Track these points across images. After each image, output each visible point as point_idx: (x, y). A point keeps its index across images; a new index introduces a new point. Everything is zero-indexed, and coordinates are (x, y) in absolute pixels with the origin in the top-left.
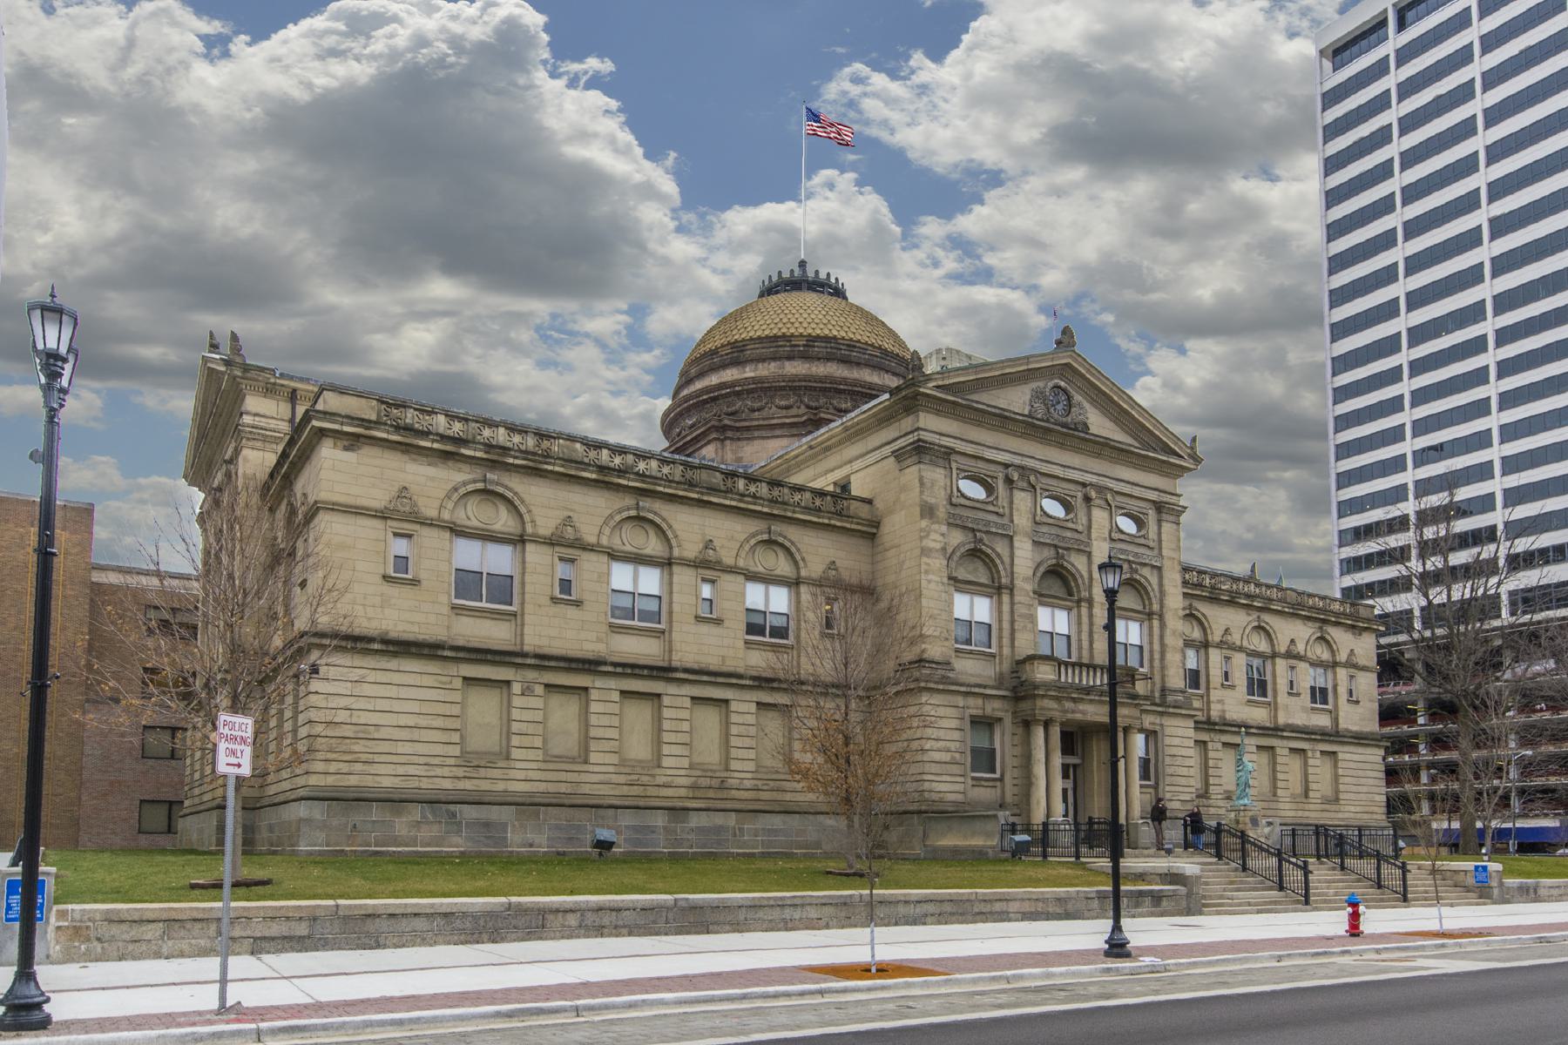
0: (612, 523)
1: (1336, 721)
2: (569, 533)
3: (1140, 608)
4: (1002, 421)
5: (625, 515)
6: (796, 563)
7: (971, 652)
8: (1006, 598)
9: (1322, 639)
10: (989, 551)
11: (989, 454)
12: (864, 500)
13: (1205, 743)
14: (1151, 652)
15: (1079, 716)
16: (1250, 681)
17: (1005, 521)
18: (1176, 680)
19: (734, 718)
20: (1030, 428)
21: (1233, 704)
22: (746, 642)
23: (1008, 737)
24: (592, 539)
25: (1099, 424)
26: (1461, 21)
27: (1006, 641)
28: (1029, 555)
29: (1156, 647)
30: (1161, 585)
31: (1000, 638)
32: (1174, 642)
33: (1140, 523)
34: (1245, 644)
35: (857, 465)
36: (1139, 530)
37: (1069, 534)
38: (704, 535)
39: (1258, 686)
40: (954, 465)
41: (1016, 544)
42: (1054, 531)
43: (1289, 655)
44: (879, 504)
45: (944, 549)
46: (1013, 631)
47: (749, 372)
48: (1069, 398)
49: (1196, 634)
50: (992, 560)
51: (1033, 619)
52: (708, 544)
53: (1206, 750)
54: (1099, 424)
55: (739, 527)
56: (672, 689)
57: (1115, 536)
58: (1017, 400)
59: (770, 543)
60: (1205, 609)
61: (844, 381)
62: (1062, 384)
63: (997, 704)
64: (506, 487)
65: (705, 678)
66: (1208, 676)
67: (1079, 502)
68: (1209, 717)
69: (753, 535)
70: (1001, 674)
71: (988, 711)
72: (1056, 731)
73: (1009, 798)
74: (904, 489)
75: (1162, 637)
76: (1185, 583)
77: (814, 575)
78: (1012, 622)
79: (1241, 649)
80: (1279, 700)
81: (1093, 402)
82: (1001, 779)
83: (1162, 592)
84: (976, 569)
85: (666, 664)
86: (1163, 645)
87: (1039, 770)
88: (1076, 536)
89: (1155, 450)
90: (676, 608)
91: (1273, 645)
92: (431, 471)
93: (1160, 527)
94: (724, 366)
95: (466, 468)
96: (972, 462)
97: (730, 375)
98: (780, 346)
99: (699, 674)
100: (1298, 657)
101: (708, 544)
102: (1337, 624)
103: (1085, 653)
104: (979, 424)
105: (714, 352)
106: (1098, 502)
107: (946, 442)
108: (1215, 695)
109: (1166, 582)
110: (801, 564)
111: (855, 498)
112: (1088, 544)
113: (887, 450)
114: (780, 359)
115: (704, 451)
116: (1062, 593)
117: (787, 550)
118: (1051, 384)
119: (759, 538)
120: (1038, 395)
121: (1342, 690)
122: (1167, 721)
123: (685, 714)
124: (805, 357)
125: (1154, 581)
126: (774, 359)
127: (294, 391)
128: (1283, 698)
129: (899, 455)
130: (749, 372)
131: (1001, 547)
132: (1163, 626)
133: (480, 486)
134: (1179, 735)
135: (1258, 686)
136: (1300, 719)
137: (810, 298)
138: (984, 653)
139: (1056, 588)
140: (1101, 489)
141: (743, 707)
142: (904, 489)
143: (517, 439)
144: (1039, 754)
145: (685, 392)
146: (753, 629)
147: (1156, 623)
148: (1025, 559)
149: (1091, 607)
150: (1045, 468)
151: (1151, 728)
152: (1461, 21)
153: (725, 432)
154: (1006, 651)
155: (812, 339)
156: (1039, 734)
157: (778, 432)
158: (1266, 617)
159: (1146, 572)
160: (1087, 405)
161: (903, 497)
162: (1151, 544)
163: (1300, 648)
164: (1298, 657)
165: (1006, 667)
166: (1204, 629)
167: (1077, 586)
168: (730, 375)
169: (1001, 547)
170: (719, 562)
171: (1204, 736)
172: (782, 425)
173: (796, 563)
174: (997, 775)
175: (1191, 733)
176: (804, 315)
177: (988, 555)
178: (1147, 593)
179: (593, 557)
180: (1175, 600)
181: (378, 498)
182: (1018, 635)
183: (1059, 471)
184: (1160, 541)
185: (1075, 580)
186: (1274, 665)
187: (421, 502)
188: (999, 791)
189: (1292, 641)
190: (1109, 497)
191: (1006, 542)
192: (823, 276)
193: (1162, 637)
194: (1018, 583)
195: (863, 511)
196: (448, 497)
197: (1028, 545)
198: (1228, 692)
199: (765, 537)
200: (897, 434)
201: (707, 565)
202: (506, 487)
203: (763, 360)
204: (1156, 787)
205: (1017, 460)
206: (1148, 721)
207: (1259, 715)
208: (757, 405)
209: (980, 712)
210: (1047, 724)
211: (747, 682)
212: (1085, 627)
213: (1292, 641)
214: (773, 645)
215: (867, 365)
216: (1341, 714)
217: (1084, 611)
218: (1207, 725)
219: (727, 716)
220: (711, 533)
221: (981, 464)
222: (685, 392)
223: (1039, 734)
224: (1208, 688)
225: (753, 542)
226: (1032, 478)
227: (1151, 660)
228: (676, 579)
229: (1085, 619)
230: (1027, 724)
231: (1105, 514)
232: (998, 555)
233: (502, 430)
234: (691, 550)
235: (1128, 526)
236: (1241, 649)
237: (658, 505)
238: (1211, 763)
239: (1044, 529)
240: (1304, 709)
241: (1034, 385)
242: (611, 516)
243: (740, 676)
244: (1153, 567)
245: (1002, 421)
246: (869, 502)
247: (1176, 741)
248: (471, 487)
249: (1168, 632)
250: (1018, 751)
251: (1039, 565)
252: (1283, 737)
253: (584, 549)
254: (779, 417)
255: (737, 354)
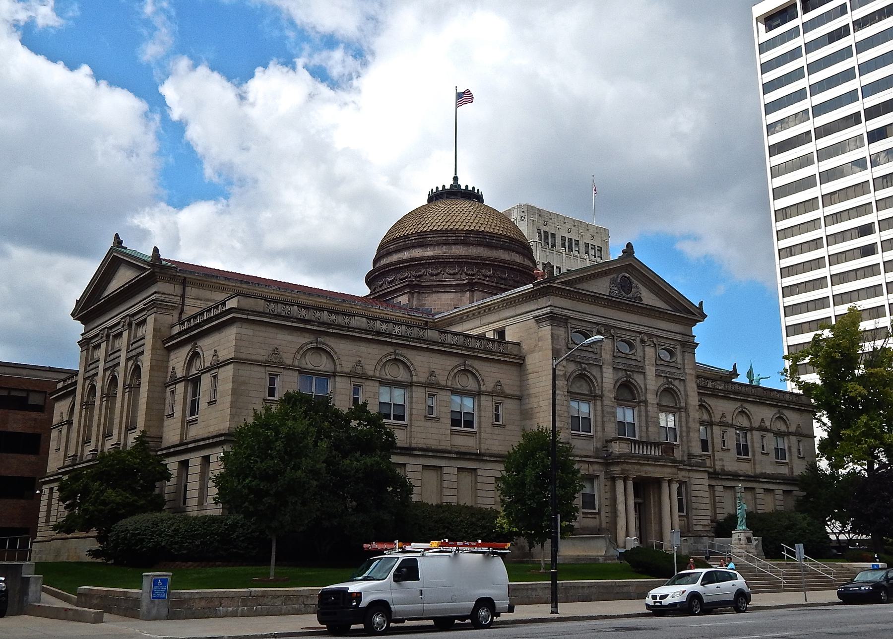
0: (381, 363)
1: (791, 469)
2: (359, 370)
3: (674, 405)
4: (595, 299)
5: (388, 358)
6: (478, 382)
7: (579, 435)
8: (599, 403)
9: (780, 418)
10: (589, 375)
11: (589, 318)
12: (514, 343)
13: (713, 486)
14: (681, 432)
15: (643, 474)
16: (738, 446)
17: (597, 357)
18: (697, 450)
19: (445, 477)
20: (609, 302)
21: (729, 462)
22: (452, 431)
23: (602, 485)
24: (371, 373)
25: (649, 298)
26: (842, 10)
27: (599, 429)
28: (611, 376)
29: (684, 429)
30: (685, 391)
31: (596, 426)
32: (694, 425)
33: (671, 353)
34: (734, 422)
35: (509, 322)
36: (671, 357)
37: (632, 362)
38: (429, 368)
39: (743, 450)
40: (569, 325)
41: (604, 370)
42: (624, 361)
43: (761, 429)
44: (524, 346)
45: (565, 374)
46: (603, 422)
47: (429, 252)
48: (631, 283)
49: (706, 417)
50: (591, 380)
51: (614, 415)
52: (432, 373)
53: (714, 491)
54: (649, 298)
55: (448, 363)
56: (412, 460)
57: (659, 362)
58: (602, 287)
59: (465, 371)
60: (711, 402)
61: (489, 259)
62: (627, 275)
63: (596, 467)
64: (327, 345)
65: (430, 454)
66: (713, 443)
67: (637, 343)
68: (715, 469)
69: (456, 367)
70: (597, 448)
71: (591, 472)
72: (630, 484)
73: (604, 525)
74: (540, 339)
75: (687, 422)
76: (699, 387)
77: (489, 390)
78: (603, 416)
79: (732, 426)
80: (756, 458)
81: (645, 285)
82: (599, 513)
83: (687, 396)
84: (581, 386)
85: (407, 446)
86: (688, 427)
87: (621, 507)
88: (637, 364)
89: (680, 312)
90: (414, 412)
91: (751, 423)
92: (289, 338)
93: (683, 356)
94: (413, 247)
95: (307, 335)
96: (579, 323)
97: (417, 253)
98: (447, 237)
99: (427, 452)
100: (766, 430)
101: (432, 373)
102: (788, 408)
103: (644, 434)
104: (583, 301)
105: (406, 237)
106: (649, 343)
107: (566, 312)
108: (718, 455)
109: (688, 388)
110: (481, 383)
111: (508, 343)
112: (643, 368)
113: (530, 316)
114: (449, 244)
115: (400, 299)
116: (629, 397)
117: (474, 374)
118: (620, 276)
119: (459, 368)
120: (613, 281)
121: (794, 450)
122: (692, 475)
123: (419, 476)
124: (465, 243)
125: (682, 389)
126: (446, 244)
127: (185, 278)
128: (759, 457)
129: (538, 320)
130: (429, 252)
131: (595, 372)
132: (688, 416)
133: (314, 345)
134: (700, 483)
135: (743, 450)
136: (770, 470)
137: (464, 205)
138: (588, 436)
139: (626, 395)
140: (650, 336)
141: (451, 471)
142: (540, 339)
143: (333, 317)
144: (620, 498)
145: (384, 262)
146: (455, 422)
147: (683, 414)
148: (608, 378)
149: (646, 406)
150: (619, 324)
151: (684, 479)
152: (842, 10)
153: (417, 288)
154: (599, 434)
155: (469, 232)
156: (620, 485)
157: (448, 289)
158: (746, 405)
159: (676, 383)
160: (640, 286)
161: (540, 344)
162: (679, 366)
163: (767, 424)
164: (766, 430)
165: (599, 445)
166: (710, 414)
167: (638, 393)
168: (417, 253)
169: (595, 372)
170: (438, 384)
171: (713, 483)
172: (451, 285)
173: (478, 382)
174: (597, 511)
175: (706, 482)
176: (461, 216)
177: (588, 377)
178: (678, 396)
179: (370, 383)
180: (694, 400)
181: (262, 354)
182: (607, 425)
183: (626, 326)
184: (684, 364)
185: (637, 390)
186: (752, 435)
187: (284, 356)
188: (598, 520)
189: (763, 419)
190: (654, 340)
191: (598, 368)
192: (470, 188)
193: (687, 422)
194: (606, 393)
195: (515, 351)
196: (298, 352)
197: (611, 370)
198: (727, 454)
199: (463, 368)
200: (536, 307)
201: (432, 386)
202: (327, 345)
203: (438, 244)
204: (687, 516)
205: (603, 321)
206: (682, 475)
207: (745, 468)
208: (434, 272)
209: (587, 473)
210: (625, 480)
211: (453, 455)
212: (644, 418)
213: (763, 419)
214: (466, 432)
215: (502, 248)
216: (795, 466)
217: (643, 408)
218: (714, 475)
219: (441, 476)
220: (433, 367)
221: (583, 324)
222: (384, 262)
223: (620, 485)
224: (713, 451)
225: (455, 371)
226: (612, 331)
227: (681, 437)
228: (414, 395)
229: (643, 414)
230: (613, 480)
231: (653, 350)
232: (594, 377)
233: (326, 313)
234: (422, 377)
235: (666, 356)
236: (732, 426)
237: (404, 352)
238: (717, 499)
239: (619, 360)
240: (771, 463)
241: (612, 276)
242: (381, 360)
243: (450, 452)
244: (681, 380)
245: (595, 299)
246: (519, 344)
247: (698, 488)
248: (309, 346)
249: (691, 420)
250: (608, 495)
251: (616, 383)
252: (760, 482)
253: (367, 379)
254: (449, 280)
255: (422, 240)
